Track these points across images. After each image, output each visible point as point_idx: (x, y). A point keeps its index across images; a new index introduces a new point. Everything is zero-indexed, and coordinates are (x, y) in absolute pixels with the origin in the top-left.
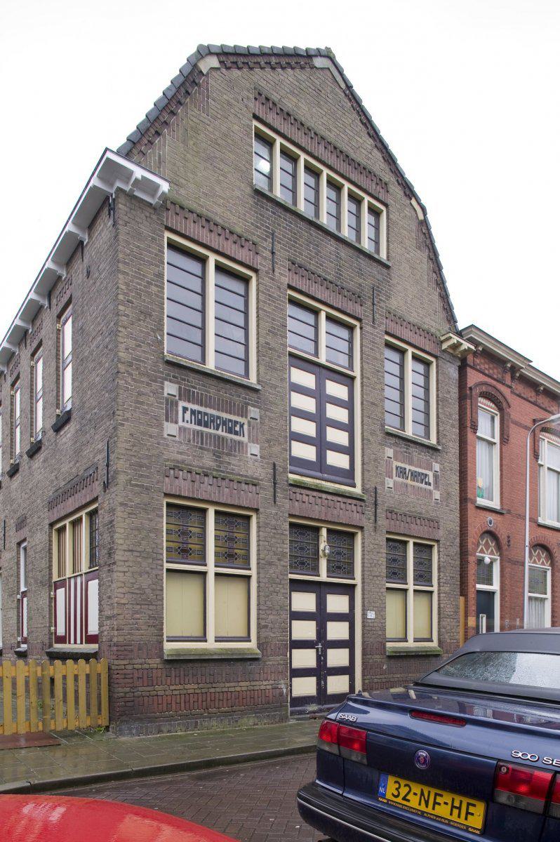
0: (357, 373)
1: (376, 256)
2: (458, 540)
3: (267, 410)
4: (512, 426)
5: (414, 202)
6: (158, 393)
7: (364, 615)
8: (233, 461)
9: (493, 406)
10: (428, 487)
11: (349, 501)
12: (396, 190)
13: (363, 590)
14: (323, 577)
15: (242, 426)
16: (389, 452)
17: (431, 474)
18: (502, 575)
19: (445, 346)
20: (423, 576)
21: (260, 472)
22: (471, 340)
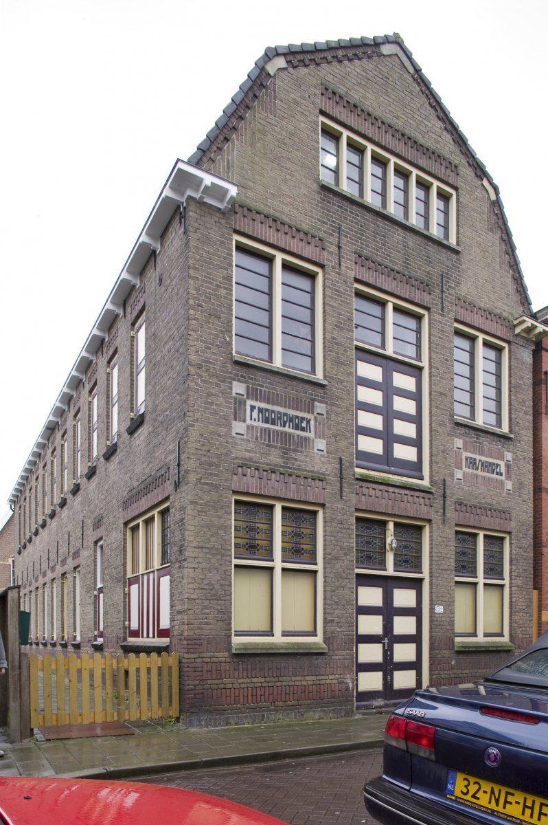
0: (425, 363)
2: (531, 532)
3: (334, 405)
5: (485, 182)
6: (226, 393)
7: (432, 609)
8: (300, 457)
10: (499, 477)
11: (417, 494)
12: (467, 171)
14: (390, 571)
15: (308, 422)
16: (459, 443)
17: (502, 464)
19: (518, 330)
20: (494, 569)
21: (327, 468)
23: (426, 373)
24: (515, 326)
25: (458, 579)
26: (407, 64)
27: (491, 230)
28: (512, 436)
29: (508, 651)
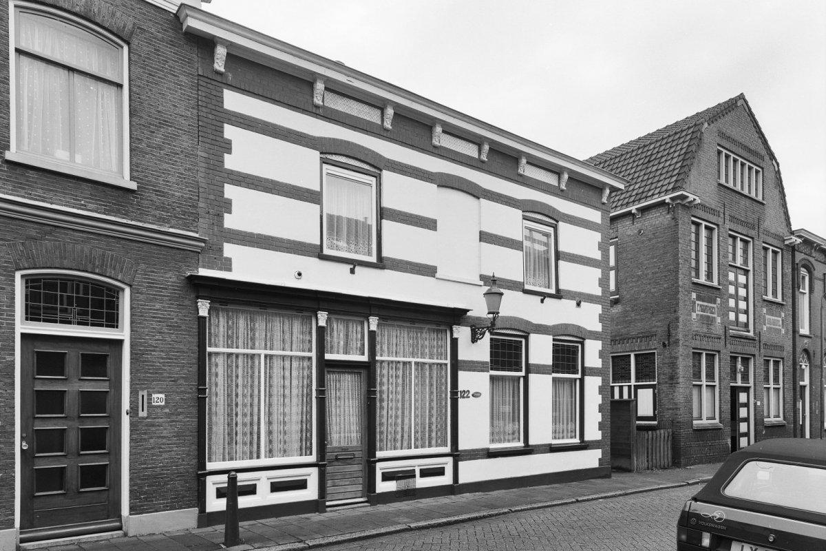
0: (750, 268)
1: (742, 192)
2: (792, 357)
4: (815, 281)
5: (774, 162)
7: (755, 404)
9: (805, 270)
12: (767, 158)
13: (755, 389)
17: (780, 319)
18: (811, 376)
19: (787, 242)
20: (710, 376)
21: (720, 332)
22: (800, 237)
23: (751, 274)
24: (785, 240)
25: (694, 383)
26: (747, 109)
27: (775, 188)
28: (785, 303)
29: (783, 426)
